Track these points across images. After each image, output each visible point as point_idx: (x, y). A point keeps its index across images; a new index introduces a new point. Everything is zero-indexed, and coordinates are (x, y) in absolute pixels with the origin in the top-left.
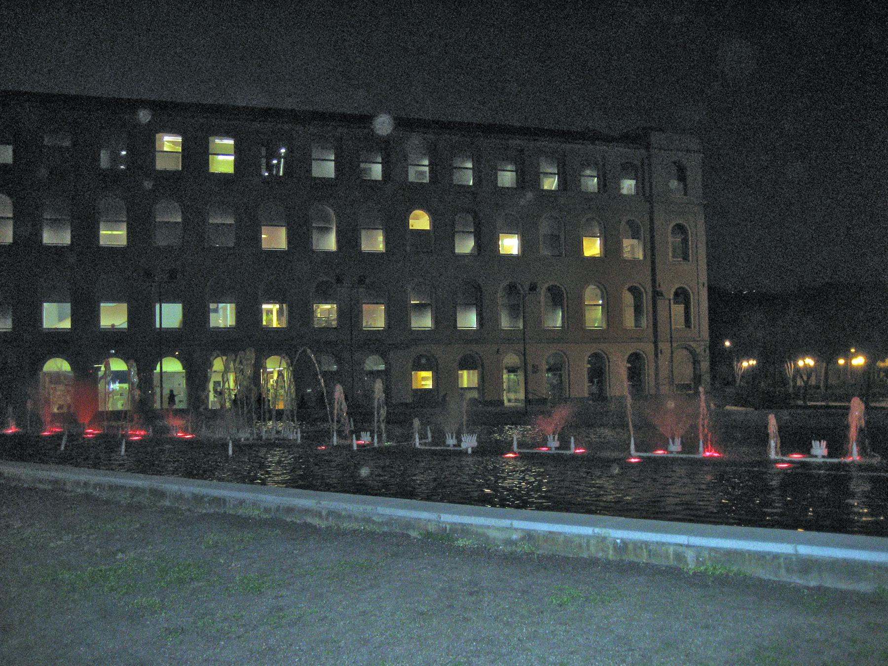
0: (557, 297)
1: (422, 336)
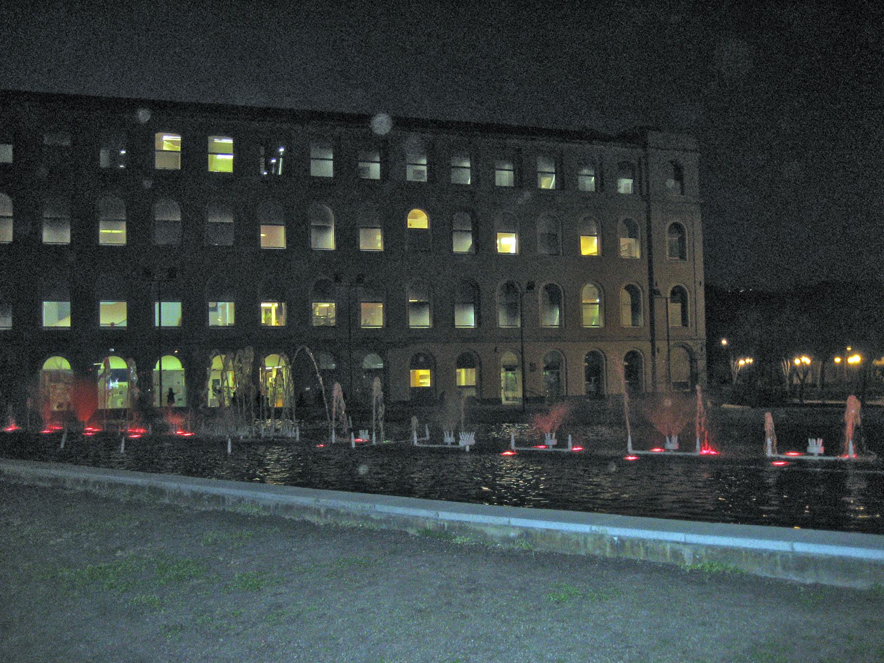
0: (554, 296)
1: (421, 335)
